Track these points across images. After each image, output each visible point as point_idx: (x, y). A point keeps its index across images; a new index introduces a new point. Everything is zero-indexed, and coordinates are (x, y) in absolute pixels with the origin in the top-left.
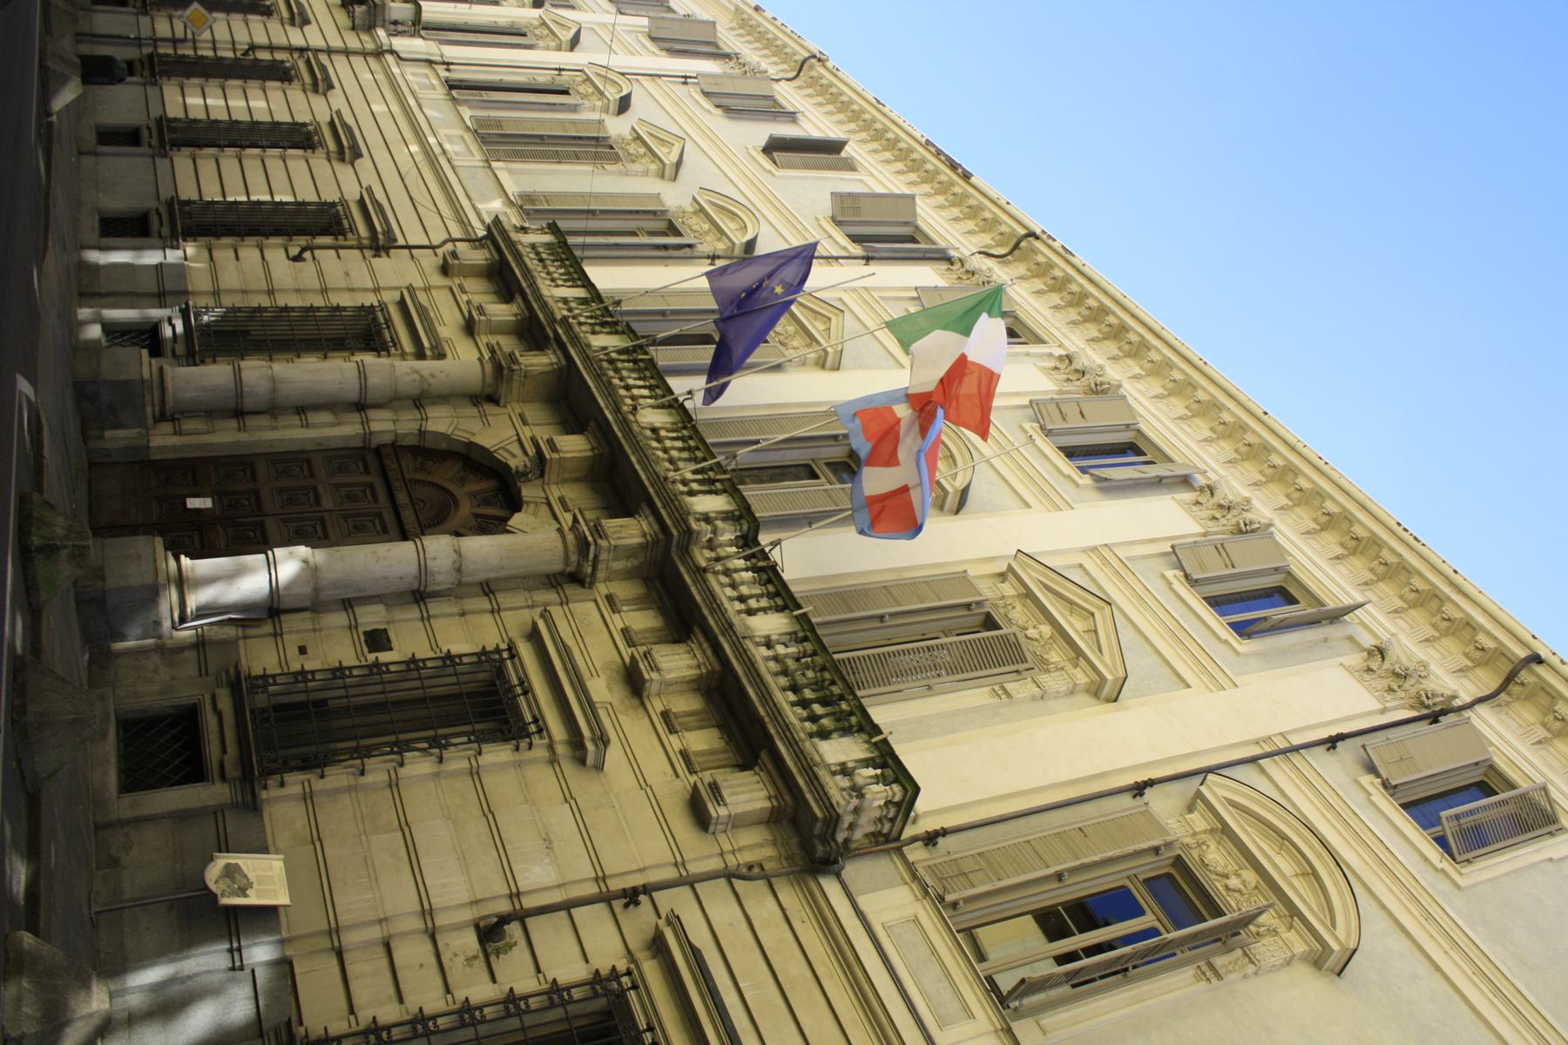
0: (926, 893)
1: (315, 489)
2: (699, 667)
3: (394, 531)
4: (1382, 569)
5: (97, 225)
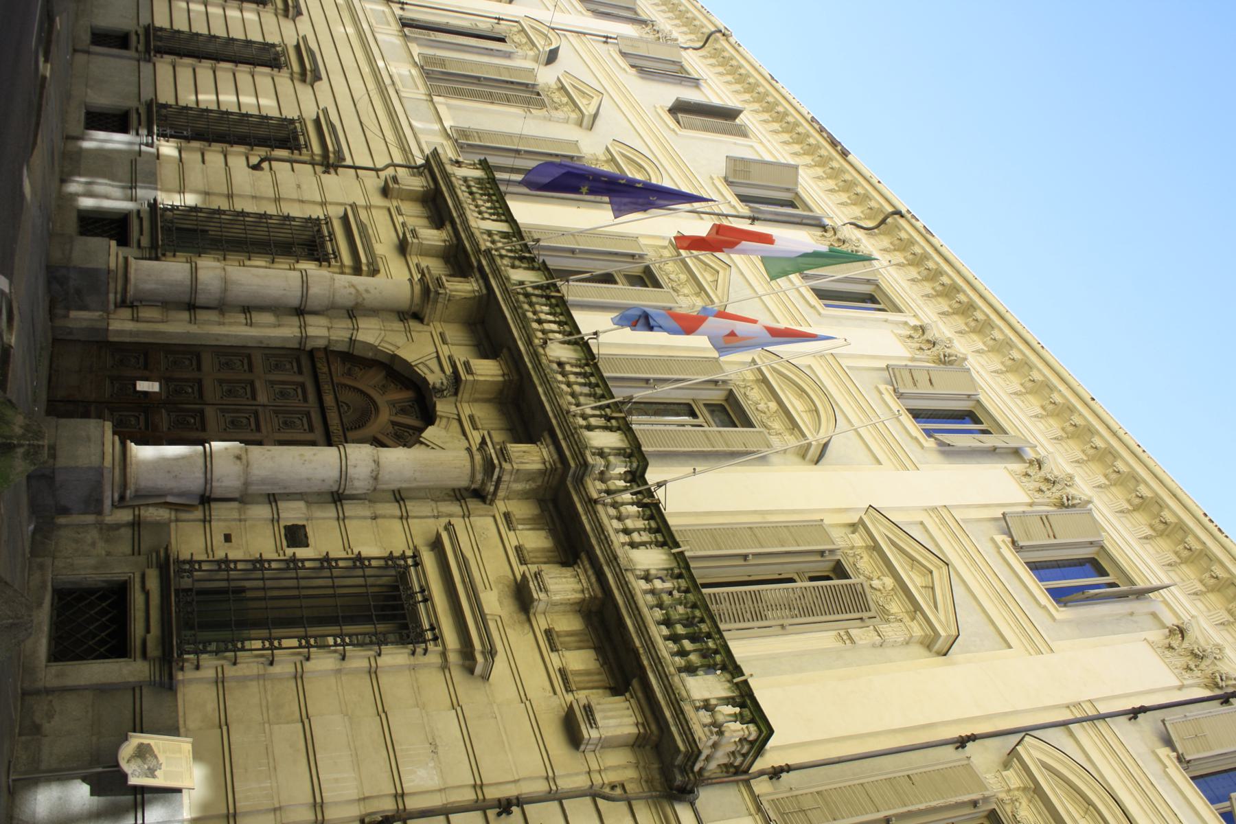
1: (252, 383)
2: (583, 591)
3: (319, 434)
4: (1186, 553)
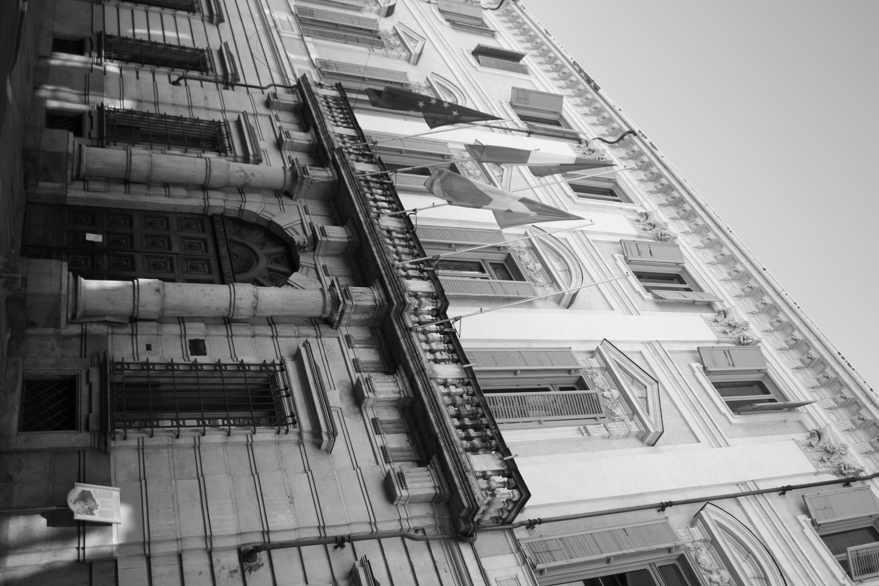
0: (525, 562)
1: (169, 238)
2: (399, 393)
3: (215, 275)
5: (51, 43)
